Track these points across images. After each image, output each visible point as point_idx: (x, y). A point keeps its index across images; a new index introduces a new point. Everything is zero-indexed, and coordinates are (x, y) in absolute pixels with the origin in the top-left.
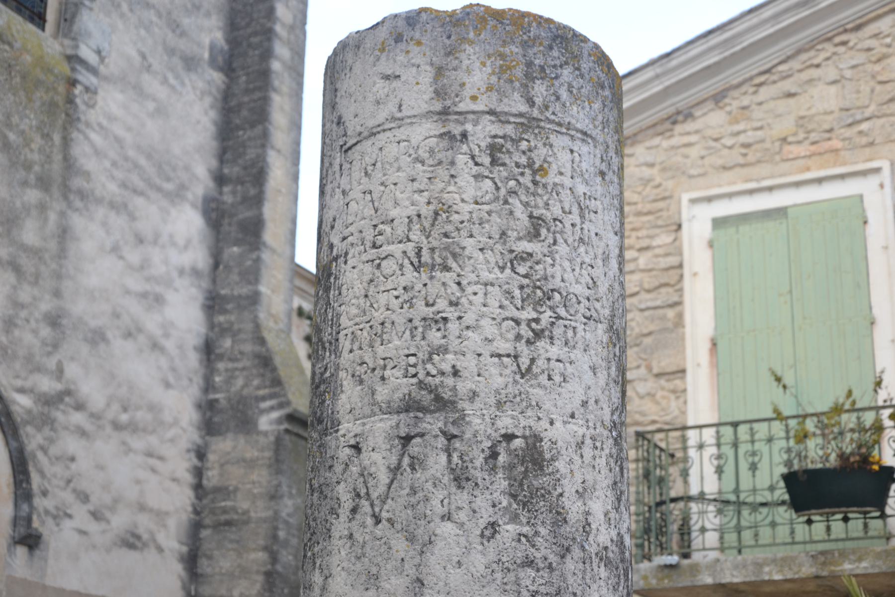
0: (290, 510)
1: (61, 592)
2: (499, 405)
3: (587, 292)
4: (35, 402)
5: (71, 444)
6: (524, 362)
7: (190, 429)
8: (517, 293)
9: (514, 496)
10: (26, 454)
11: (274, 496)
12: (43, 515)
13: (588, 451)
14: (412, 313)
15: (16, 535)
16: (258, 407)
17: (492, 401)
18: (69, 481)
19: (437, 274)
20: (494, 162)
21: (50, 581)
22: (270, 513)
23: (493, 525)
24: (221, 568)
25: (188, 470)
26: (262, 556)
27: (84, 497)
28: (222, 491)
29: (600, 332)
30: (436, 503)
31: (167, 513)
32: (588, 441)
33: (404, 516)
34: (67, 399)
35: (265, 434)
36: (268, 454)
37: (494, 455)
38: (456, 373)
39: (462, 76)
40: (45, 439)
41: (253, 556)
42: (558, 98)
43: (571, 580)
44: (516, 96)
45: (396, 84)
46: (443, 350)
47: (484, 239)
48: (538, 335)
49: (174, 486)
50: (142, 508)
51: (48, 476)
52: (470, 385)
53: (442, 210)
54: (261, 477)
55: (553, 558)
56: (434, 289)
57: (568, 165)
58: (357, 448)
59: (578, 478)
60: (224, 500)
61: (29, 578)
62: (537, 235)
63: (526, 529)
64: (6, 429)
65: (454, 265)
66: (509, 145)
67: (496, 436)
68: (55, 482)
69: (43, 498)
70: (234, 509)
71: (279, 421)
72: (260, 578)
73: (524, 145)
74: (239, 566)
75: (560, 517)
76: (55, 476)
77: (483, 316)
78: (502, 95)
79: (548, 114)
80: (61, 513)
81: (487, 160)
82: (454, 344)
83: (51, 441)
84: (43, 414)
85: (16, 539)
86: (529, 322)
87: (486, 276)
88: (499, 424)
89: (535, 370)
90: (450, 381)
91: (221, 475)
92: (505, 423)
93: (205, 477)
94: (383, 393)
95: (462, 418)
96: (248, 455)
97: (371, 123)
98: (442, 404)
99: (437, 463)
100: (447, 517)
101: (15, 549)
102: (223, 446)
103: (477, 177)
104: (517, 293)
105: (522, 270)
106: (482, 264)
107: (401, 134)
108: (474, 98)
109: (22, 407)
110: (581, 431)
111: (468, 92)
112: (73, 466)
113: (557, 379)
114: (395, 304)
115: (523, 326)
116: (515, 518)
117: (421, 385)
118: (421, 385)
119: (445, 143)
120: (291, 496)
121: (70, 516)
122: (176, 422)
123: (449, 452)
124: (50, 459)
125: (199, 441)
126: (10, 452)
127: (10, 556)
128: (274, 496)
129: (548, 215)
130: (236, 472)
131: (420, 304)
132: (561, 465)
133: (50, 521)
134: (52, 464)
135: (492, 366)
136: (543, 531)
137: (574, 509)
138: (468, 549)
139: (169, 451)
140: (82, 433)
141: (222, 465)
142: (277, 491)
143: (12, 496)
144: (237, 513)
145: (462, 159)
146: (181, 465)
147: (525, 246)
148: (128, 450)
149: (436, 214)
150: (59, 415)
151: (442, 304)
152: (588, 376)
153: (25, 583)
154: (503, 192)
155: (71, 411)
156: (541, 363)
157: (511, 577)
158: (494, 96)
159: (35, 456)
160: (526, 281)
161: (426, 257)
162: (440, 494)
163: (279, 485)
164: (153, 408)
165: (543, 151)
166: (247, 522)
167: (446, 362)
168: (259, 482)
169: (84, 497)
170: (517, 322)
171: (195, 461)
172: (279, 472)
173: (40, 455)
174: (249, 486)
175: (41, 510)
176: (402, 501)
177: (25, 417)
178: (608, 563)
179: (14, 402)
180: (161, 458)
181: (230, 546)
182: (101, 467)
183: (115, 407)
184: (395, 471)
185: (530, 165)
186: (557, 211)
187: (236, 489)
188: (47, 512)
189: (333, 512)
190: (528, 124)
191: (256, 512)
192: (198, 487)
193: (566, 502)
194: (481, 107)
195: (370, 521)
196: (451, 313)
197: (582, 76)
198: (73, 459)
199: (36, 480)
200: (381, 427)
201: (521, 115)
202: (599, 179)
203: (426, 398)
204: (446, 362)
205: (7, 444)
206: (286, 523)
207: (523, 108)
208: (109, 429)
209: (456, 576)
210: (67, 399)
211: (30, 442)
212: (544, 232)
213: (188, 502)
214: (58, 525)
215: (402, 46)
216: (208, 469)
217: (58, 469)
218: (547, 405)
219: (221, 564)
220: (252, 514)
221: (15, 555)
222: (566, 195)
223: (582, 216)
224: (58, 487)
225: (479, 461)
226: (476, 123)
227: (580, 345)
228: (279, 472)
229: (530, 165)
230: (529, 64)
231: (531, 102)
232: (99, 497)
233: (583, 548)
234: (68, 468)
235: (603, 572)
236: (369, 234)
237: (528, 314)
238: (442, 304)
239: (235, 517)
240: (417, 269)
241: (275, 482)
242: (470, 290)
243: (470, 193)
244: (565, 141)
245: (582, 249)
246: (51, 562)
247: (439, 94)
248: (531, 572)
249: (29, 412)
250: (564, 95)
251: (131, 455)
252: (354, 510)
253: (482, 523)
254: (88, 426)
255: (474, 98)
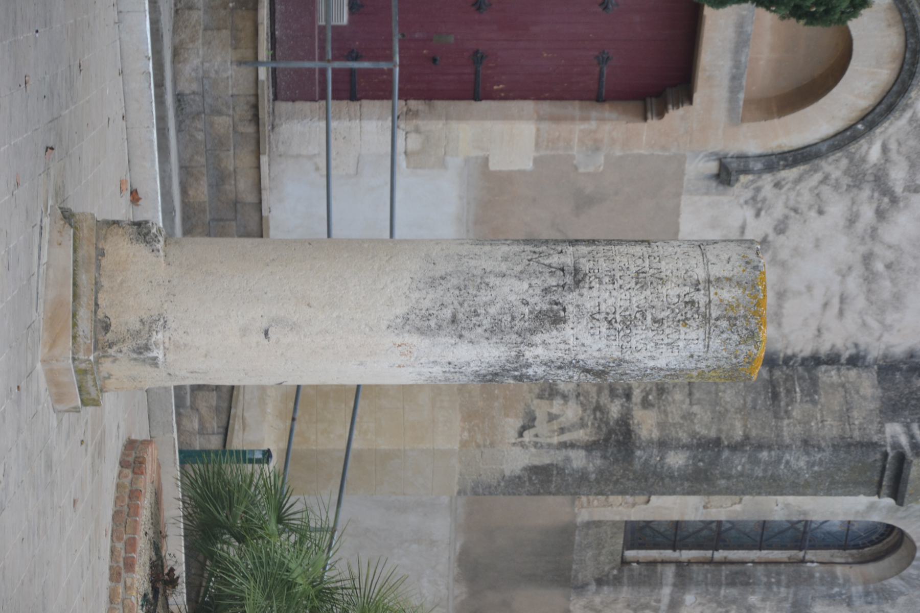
0: (794, 465)
1: (677, 213)
2: (578, 306)
3: (633, 347)
4: (875, 165)
5: (837, 209)
6: (597, 316)
7: (883, 346)
8: (627, 313)
9: (540, 312)
10: (816, 162)
11: (806, 444)
12: (755, 185)
13: (562, 346)
14: (617, 270)
15: (729, 160)
16: (912, 421)
17: (579, 303)
18: (796, 210)
19: (634, 280)
20: (686, 303)
21: (685, 200)
22: (788, 441)
23: (528, 304)
24: (724, 392)
25: (833, 346)
26: (738, 434)
27: (781, 228)
28: (813, 388)
29: (617, 353)
30: (536, 281)
31: (780, 325)
32: (567, 347)
33: (531, 270)
34: (886, 200)
35: (881, 431)
36: (857, 434)
37: (556, 304)
38: (591, 288)
39: (727, 288)
40: (837, 180)
41: (738, 425)
42: (722, 333)
43: (508, 337)
44: (719, 313)
45: (725, 262)
46: (600, 283)
47: (650, 299)
48: (610, 322)
49: (811, 332)
50: (781, 295)
51: (798, 188)
52: (586, 294)
53: (663, 281)
54: (830, 429)
55: (516, 328)
56: (627, 279)
57: (690, 337)
58: (561, 252)
59: (551, 341)
60: (802, 391)
61: (686, 178)
62: (655, 322)
63: (527, 317)
64: (838, 137)
65: (638, 286)
66: (695, 309)
67: (564, 304)
68: (792, 195)
69: (772, 184)
70: (792, 401)
71: (896, 445)
72: (713, 434)
73: (696, 316)
74: (727, 410)
75: (533, 332)
76: (799, 194)
77: (616, 298)
78: (719, 306)
79: (713, 328)
80: (759, 205)
81: (687, 299)
82: (603, 287)
83: (836, 187)
84: (865, 175)
85: (723, 160)
86: (615, 318)
87: (634, 300)
88: (570, 306)
89: (594, 321)
90: (587, 286)
91: (832, 385)
92: (570, 308)
93: (829, 367)
94: (583, 261)
95: (571, 290)
96: (855, 414)
97: (708, 254)
98: (577, 283)
99: (553, 282)
100: (530, 286)
101: (714, 160)
102: (867, 385)
103: (679, 296)
104: (627, 313)
105: (638, 315)
106: (639, 298)
107: (701, 265)
108: (716, 294)
109: (867, 152)
110: (571, 342)
111: (719, 291)
112: (813, 214)
113: (592, 331)
114: (622, 264)
115: (613, 316)
116: (531, 312)
117: (586, 275)
118: (586, 275)
119: (694, 282)
120: (811, 465)
121: (758, 215)
122: (887, 328)
123: (558, 286)
124: (816, 188)
125: (870, 358)
126: (816, 144)
127: (706, 156)
128: (806, 444)
129: (665, 327)
130: (836, 401)
131: (621, 273)
132: (555, 332)
133: (749, 194)
134: (811, 190)
135: (594, 303)
136: (526, 324)
137: (537, 339)
138: (517, 294)
139: (851, 322)
140: (852, 221)
141: (843, 386)
142: (813, 446)
143: (770, 152)
144: (787, 405)
145: (687, 289)
146: (838, 336)
147: (649, 317)
148: (844, 273)
149: (661, 279)
150: (866, 192)
151: (621, 282)
152: (595, 347)
153: (680, 173)
154: (673, 307)
155: (875, 206)
156: (597, 324)
157: (507, 311)
158: (718, 303)
159: (816, 171)
160: (633, 317)
161: (641, 275)
162: (539, 283)
163: (820, 449)
164: (898, 299)
165: (694, 325)
166: (776, 416)
167: (595, 284)
168: (823, 426)
169: (781, 228)
170: (614, 313)
171: (846, 355)
172: (835, 447)
173: (818, 176)
174: (819, 416)
175: (760, 183)
176: (537, 269)
177: (857, 156)
178: (518, 357)
179: (871, 143)
180: (841, 313)
181: (749, 399)
182: (817, 244)
183: (890, 255)
184: (550, 266)
185: (687, 319)
186: (667, 331)
187: (814, 402)
188: (758, 190)
189: (535, 246)
190: (706, 318)
191: (788, 425)
192: (816, 361)
193: (540, 335)
194: (712, 297)
195: (529, 258)
196: (617, 286)
197: (737, 345)
198: (821, 212)
199: (791, 174)
200: (568, 260)
201: (710, 315)
202: (689, 354)
203: (580, 277)
204: (595, 284)
205: (824, 141)
206: (779, 461)
207: (714, 315)
208: (862, 249)
209: (506, 289)
210: (886, 200)
211: (830, 164)
212: (657, 325)
213: (797, 350)
214: (746, 202)
215: (744, 264)
216: (839, 370)
217: (807, 197)
218: (580, 327)
219: (729, 392)
220: (786, 422)
221: (708, 161)
222: (675, 336)
223: (668, 344)
224: (788, 199)
225: (553, 298)
226: (705, 295)
227: (609, 343)
228: (835, 447)
229: (687, 319)
230: (736, 319)
231: (717, 319)
232: (784, 245)
233: (522, 343)
234: (810, 208)
235: (513, 354)
236: (656, 254)
237: (619, 319)
238: (621, 282)
239: (783, 404)
240: (637, 272)
241: (823, 444)
242: (627, 293)
243: (671, 292)
244: (702, 336)
245: (652, 344)
246: (706, 199)
247: (718, 279)
248: (509, 319)
249: (863, 160)
250: (725, 336)
251: (839, 278)
252: (535, 252)
253: (528, 299)
254: (860, 226)
255: (716, 294)
